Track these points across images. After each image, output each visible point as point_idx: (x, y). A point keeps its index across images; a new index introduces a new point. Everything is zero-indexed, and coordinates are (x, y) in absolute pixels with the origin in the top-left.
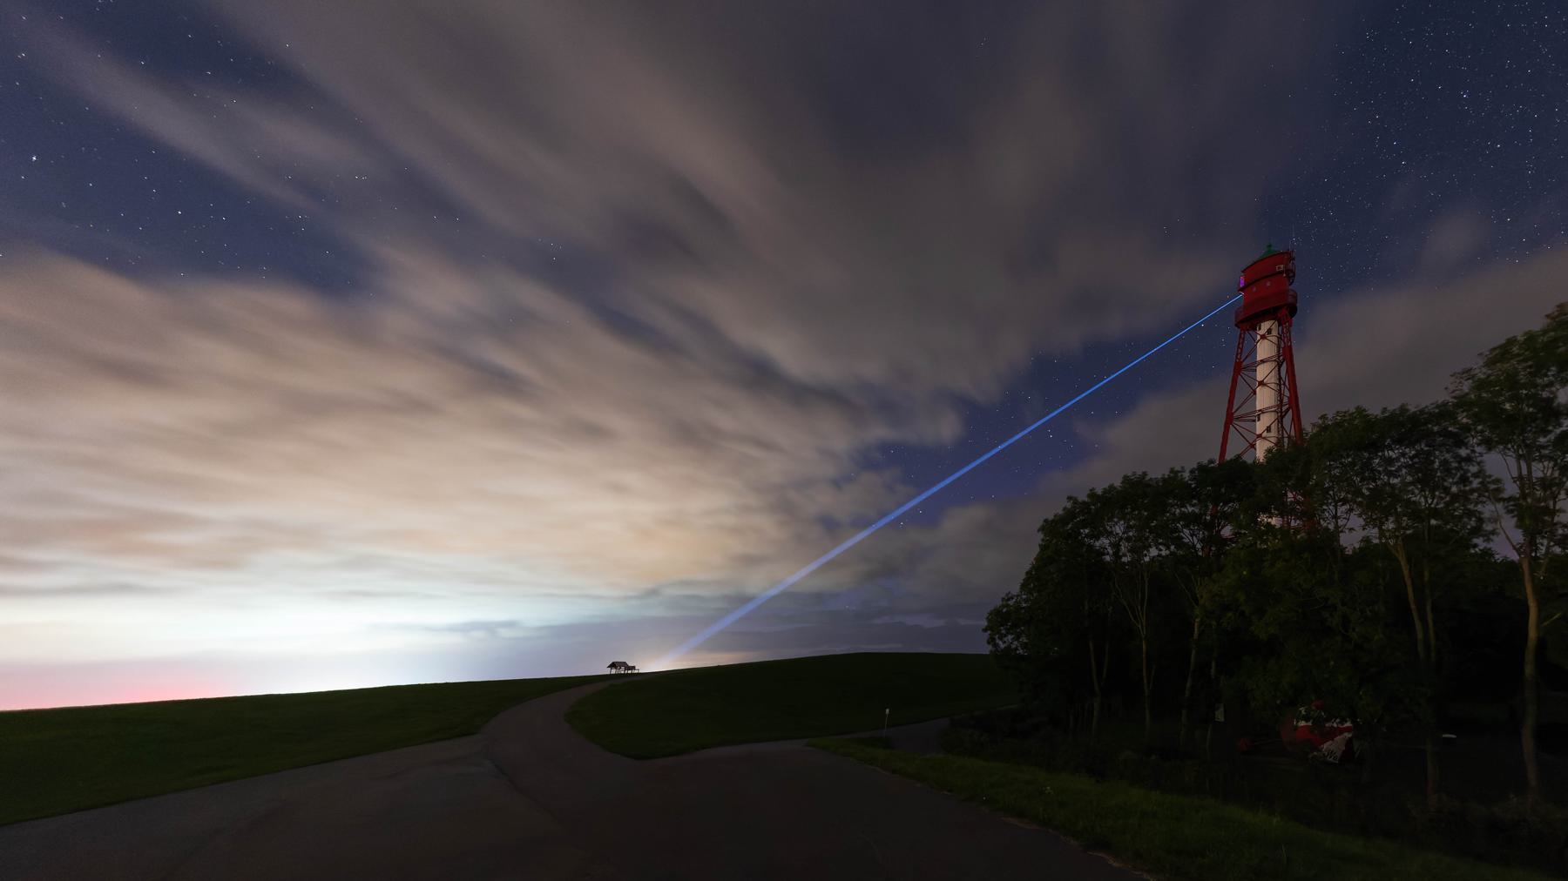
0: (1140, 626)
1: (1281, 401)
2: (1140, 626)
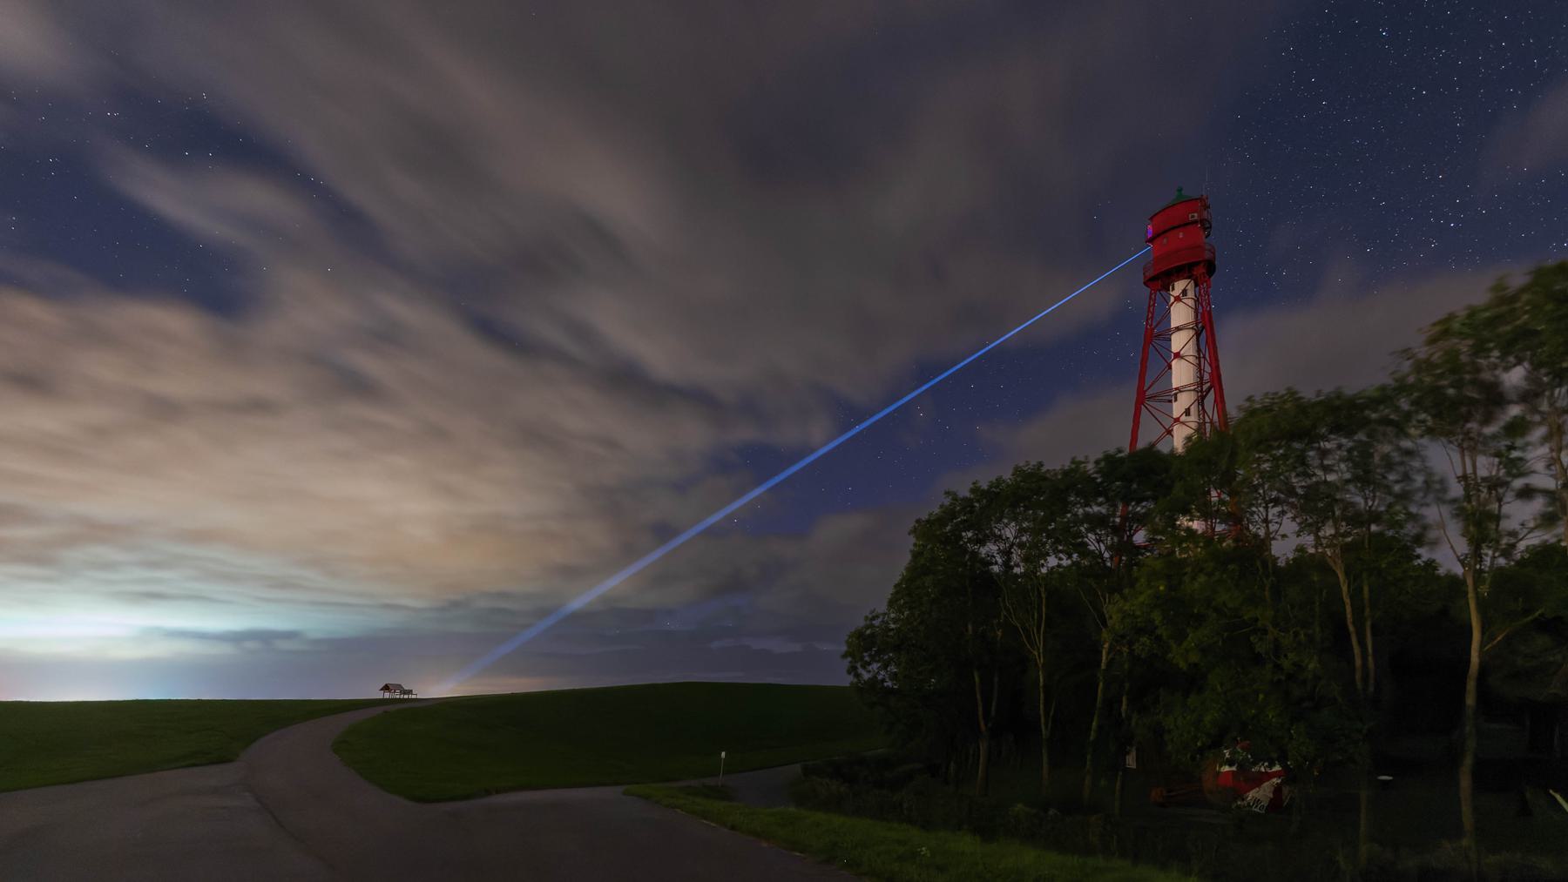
0: (1036, 653)
1: (1201, 378)
2: (1036, 653)
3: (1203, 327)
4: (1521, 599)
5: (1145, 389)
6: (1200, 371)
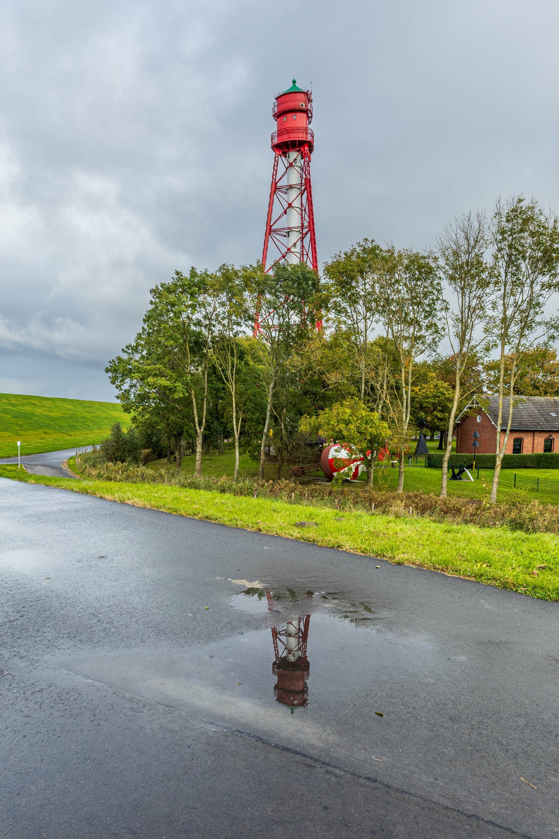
1: (302, 226)
2: (231, 387)
3: (305, 189)
6: (302, 219)
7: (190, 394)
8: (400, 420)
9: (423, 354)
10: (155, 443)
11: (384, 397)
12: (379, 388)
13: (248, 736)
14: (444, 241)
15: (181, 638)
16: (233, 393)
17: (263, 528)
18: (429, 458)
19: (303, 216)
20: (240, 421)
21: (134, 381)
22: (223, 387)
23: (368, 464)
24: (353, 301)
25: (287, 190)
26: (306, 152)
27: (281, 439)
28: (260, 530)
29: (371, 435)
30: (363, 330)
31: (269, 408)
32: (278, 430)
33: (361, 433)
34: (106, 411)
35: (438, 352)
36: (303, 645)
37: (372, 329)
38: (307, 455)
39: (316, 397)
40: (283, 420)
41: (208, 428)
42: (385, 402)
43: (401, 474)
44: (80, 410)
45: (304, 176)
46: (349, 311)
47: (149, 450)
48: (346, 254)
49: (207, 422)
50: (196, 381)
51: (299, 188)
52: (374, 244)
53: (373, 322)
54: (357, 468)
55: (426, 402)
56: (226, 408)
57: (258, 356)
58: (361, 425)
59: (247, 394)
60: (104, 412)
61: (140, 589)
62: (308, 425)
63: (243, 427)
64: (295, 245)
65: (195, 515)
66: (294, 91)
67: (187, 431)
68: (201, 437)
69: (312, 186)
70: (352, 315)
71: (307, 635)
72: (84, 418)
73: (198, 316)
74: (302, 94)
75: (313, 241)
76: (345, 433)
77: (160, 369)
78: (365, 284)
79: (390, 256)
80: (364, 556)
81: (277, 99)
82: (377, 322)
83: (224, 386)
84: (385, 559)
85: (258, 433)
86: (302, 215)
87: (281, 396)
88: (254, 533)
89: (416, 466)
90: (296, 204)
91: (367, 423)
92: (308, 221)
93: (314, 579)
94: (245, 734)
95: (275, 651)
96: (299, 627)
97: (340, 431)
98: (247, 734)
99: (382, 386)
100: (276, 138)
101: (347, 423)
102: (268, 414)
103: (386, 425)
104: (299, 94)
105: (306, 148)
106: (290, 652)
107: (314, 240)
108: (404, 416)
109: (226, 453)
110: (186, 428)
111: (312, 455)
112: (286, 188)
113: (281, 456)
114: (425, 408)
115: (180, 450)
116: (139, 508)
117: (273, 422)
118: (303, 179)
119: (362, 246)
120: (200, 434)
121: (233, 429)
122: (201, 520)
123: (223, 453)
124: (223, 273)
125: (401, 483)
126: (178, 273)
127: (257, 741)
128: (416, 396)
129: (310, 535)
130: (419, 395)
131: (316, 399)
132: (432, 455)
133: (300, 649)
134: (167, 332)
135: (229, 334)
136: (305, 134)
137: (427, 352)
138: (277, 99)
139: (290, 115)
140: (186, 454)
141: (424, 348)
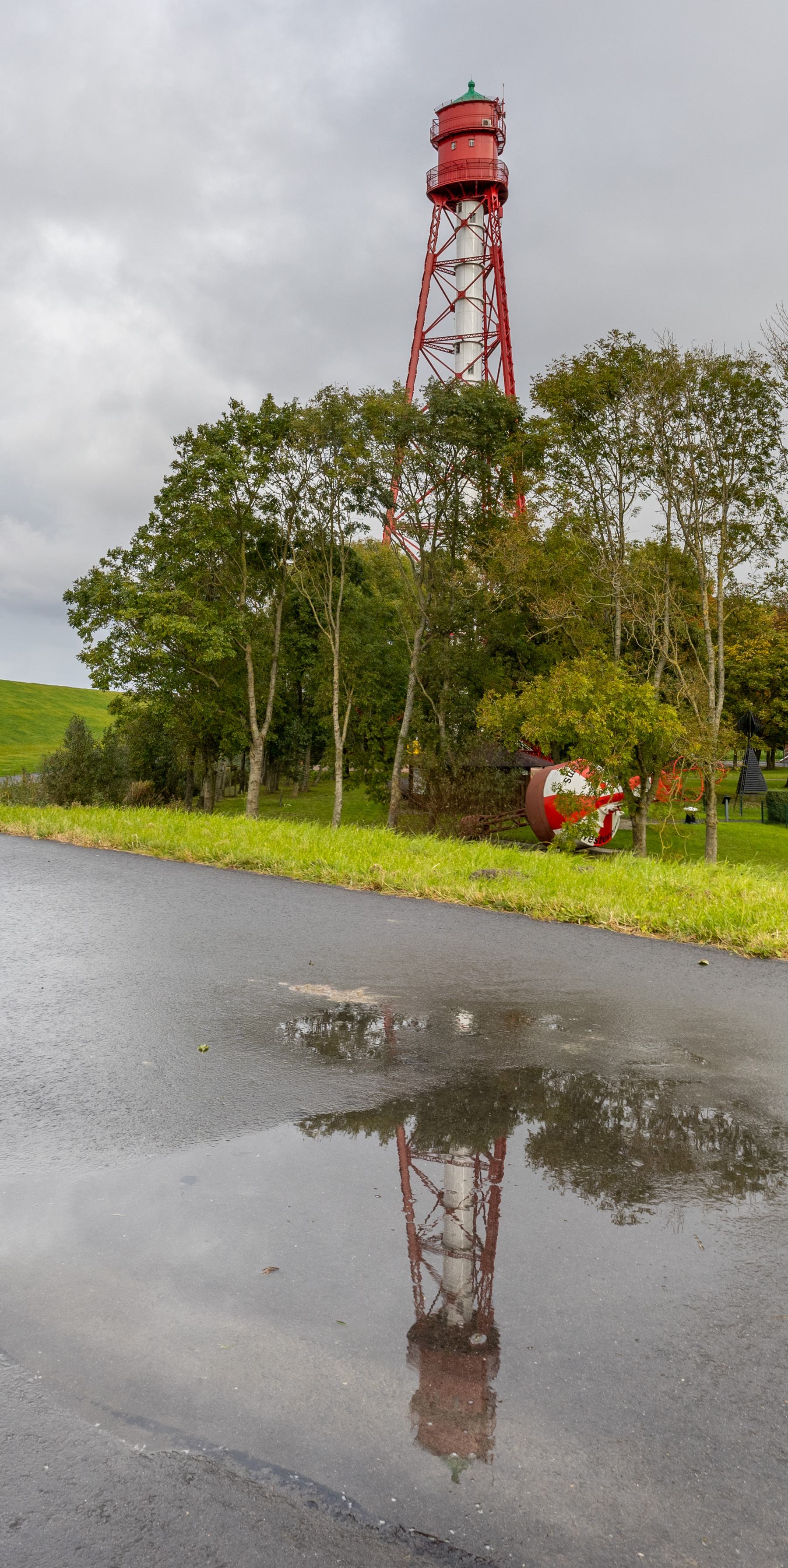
0: (330, 637)
1: (486, 329)
2: (330, 637)
3: (491, 266)
4: (266, 598)
5: (424, 330)
6: (485, 321)
7: (241, 655)
8: (704, 705)
9: (746, 563)
10: (160, 768)
11: (666, 652)
12: (654, 632)
13: (276, 1479)
14: (778, 332)
15: (104, 1123)
16: (335, 650)
17: (387, 881)
18: (770, 801)
19: (488, 315)
20: (348, 712)
21: (123, 625)
22: (313, 646)
23: (635, 808)
24: (590, 453)
25: (455, 268)
26: (493, 201)
27: (438, 751)
28: (378, 887)
29: (640, 734)
30: (616, 512)
31: (412, 682)
32: (431, 730)
33: (617, 731)
34: (66, 704)
35: (780, 557)
36: (482, 1279)
37: (635, 511)
38: (495, 786)
39: (517, 661)
40: (442, 707)
41: (278, 729)
42: (667, 664)
43: (711, 831)
44: (9, 701)
45: (490, 243)
46: (586, 473)
47: (147, 783)
48: (575, 362)
49: (276, 715)
50: (256, 624)
51: (479, 265)
52: (633, 341)
53: (637, 496)
54: (608, 819)
55: (756, 679)
56: (319, 684)
57: (392, 582)
58: (617, 712)
59: (364, 652)
60: (61, 707)
61: (20, 1001)
62: (498, 714)
63: (353, 723)
64: (470, 369)
65: (217, 858)
66: (471, 99)
67: (229, 735)
68: (261, 748)
69: (504, 259)
70: (593, 482)
71: (492, 1254)
72: (16, 717)
73: (270, 489)
74: (487, 105)
75: (507, 360)
76: (581, 730)
77: (180, 599)
78: (617, 420)
79: (669, 363)
80: (660, 941)
81: (439, 113)
82: (644, 496)
83: (314, 642)
84: (719, 946)
85: (386, 739)
86: (485, 312)
87: (439, 654)
88: (361, 892)
89: (740, 820)
90: (474, 292)
91: (629, 708)
92: (497, 322)
93: (525, 985)
94: (265, 1471)
95: (415, 1297)
96: (474, 1230)
97: (571, 727)
98: (277, 1470)
99: (660, 629)
100: (437, 178)
101: (584, 707)
102: (410, 694)
103: (672, 711)
104: (481, 104)
105: (494, 195)
106: (451, 1298)
107: (510, 357)
108: (712, 697)
109: (315, 792)
110: (227, 728)
111: (507, 787)
112: (454, 265)
113: (438, 790)
114: (754, 690)
115: (214, 782)
116: (83, 848)
117: (420, 712)
118: (488, 249)
119: (607, 346)
120: (258, 742)
121: (332, 728)
122: (231, 867)
123: (309, 791)
124: (324, 404)
125: (713, 851)
126: (235, 405)
127: (312, 1504)
128: (732, 665)
129: (510, 894)
130: (738, 662)
131: (516, 665)
132: (777, 794)
133: (476, 1293)
134: (201, 522)
135: (332, 527)
136: (491, 171)
137: (755, 556)
138: (439, 113)
139: (463, 140)
140: (226, 794)
141: (748, 549)
